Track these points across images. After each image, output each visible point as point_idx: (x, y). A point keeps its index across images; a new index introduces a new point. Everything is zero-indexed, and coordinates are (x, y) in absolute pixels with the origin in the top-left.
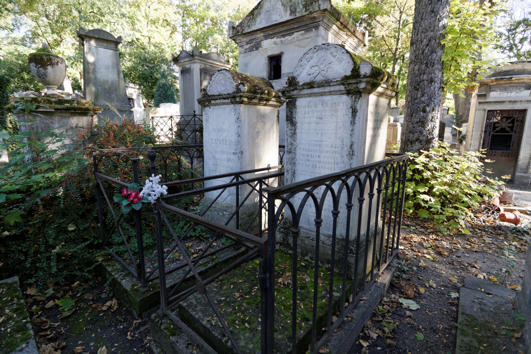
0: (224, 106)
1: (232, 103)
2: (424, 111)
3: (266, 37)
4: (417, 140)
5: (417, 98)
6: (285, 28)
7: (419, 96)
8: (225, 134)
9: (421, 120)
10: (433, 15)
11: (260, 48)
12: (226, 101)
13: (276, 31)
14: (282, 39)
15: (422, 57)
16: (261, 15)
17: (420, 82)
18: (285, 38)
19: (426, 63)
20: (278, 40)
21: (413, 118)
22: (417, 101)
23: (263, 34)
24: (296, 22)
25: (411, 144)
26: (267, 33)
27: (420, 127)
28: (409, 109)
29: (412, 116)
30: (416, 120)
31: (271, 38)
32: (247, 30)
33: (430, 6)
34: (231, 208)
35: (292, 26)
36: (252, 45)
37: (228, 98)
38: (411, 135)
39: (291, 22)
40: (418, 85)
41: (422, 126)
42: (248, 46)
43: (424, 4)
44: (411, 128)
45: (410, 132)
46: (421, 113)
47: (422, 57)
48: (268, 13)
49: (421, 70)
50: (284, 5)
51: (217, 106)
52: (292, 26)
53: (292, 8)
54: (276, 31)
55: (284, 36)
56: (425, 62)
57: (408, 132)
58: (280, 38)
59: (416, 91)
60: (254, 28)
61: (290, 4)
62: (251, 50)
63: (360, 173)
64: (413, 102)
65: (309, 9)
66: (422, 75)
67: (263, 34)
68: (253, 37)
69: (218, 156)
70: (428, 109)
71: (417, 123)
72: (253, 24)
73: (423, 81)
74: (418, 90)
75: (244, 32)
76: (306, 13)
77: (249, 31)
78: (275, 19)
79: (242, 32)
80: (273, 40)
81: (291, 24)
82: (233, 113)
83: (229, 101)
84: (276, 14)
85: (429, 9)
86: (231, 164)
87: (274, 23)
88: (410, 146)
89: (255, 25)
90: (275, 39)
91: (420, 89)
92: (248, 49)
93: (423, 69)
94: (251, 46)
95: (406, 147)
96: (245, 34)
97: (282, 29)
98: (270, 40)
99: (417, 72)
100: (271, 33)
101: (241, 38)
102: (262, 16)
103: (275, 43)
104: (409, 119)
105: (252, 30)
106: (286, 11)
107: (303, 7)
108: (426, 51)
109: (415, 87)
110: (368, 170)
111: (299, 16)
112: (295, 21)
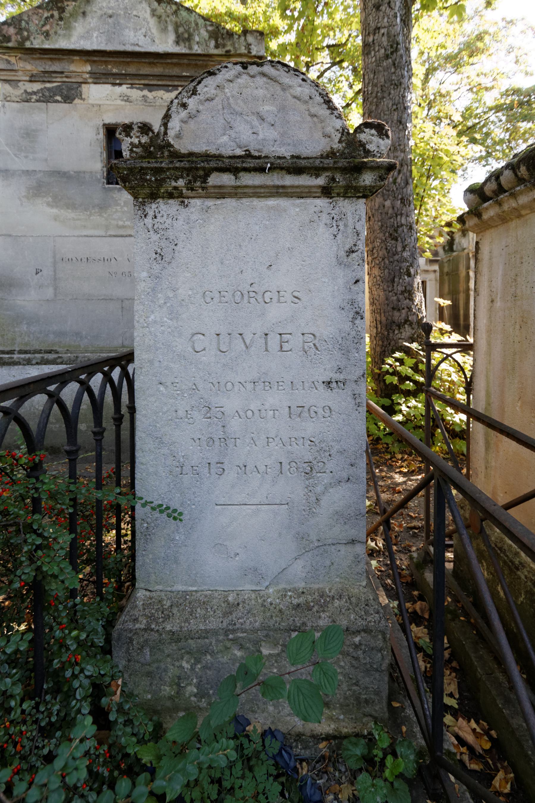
0: (272, 202)
1: (326, 192)
2: (409, 275)
3: (99, 78)
4: (405, 323)
5: (396, 253)
6: (158, 70)
7: (399, 249)
8: (276, 312)
9: (408, 289)
10: (401, 127)
11: (77, 101)
12: (304, 180)
13: (132, 70)
14: (146, 92)
15: (395, 189)
16: (89, 19)
17: (398, 227)
18: (154, 93)
19: (401, 199)
20: (136, 94)
21: (395, 285)
22: (396, 257)
23: (88, 68)
24: (188, 65)
25: (399, 329)
26: (101, 68)
27: (408, 300)
28: (386, 271)
29: (393, 281)
30: (400, 288)
31: (114, 84)
32: (37, 42)
33: (396, 113)
34: (323, 607)
35: (176, 71)
36: (48, 85)
37: (316, 171)
38: (396, 314)
39: (175, 61)
40: (396, 231)
41: (409, 299)
42: (36, 87)
43: (385, 108)
44: (395, 302)
45: (393, 309)
46: (406, 277)
47: (395, 189)
48: (110, 20)
49: (396, 209)
50: (160, 17)
51: (230, 203)
52: (176, 71)
53: (181, 30)
54: (132, 70)
55: (150, 87)
56: (400, 196)
57: (389, 308)
58: (142, 90)
59: (393, 242)
60: (63, 44)
61: (174, 18)
62: (46, 98)
63: (91, 375)
64: (391, 260)
65: (224, 46)
66: (399, 217)
67: (88, 68)
68: (56, 67)
69: (231, 403)
70: (412, 271)
71: (402, 293)
72: (60, 32)
73: (402, 225)
74: (397, 240)
75: (28, 45)
76: (216, 52)
77: (47, 46)
78: (133, 40)
79: (21, 44)
80: (118, 90)
81: (175, 64)
82: (323, 233)
83: (321, 181)
84: (136, 30)
85: (395, 117)
86: (310, 428)
87: (129, 48)
88: (396, 332)
89: (68, 36)
90: (124, 89)
91: (399, 239)
92: (34, 93)
93: (399, 206)
94: (49, 89)
95: (391, 335)
96: (32, 51)
97: (146, 70)
98: (109, 87)
99: (390, 211)
100: (115, 71)
101: (13, 60)
102: (92, 21)
103: (127, 99)
104: (388, 287)
105: (57, 46)
106: (164, 30)
107: (210, 37)
108: (399, 180)
109: (391, 235)
110: (106, 369)
111: (199, 52)
112: (185, 61)
